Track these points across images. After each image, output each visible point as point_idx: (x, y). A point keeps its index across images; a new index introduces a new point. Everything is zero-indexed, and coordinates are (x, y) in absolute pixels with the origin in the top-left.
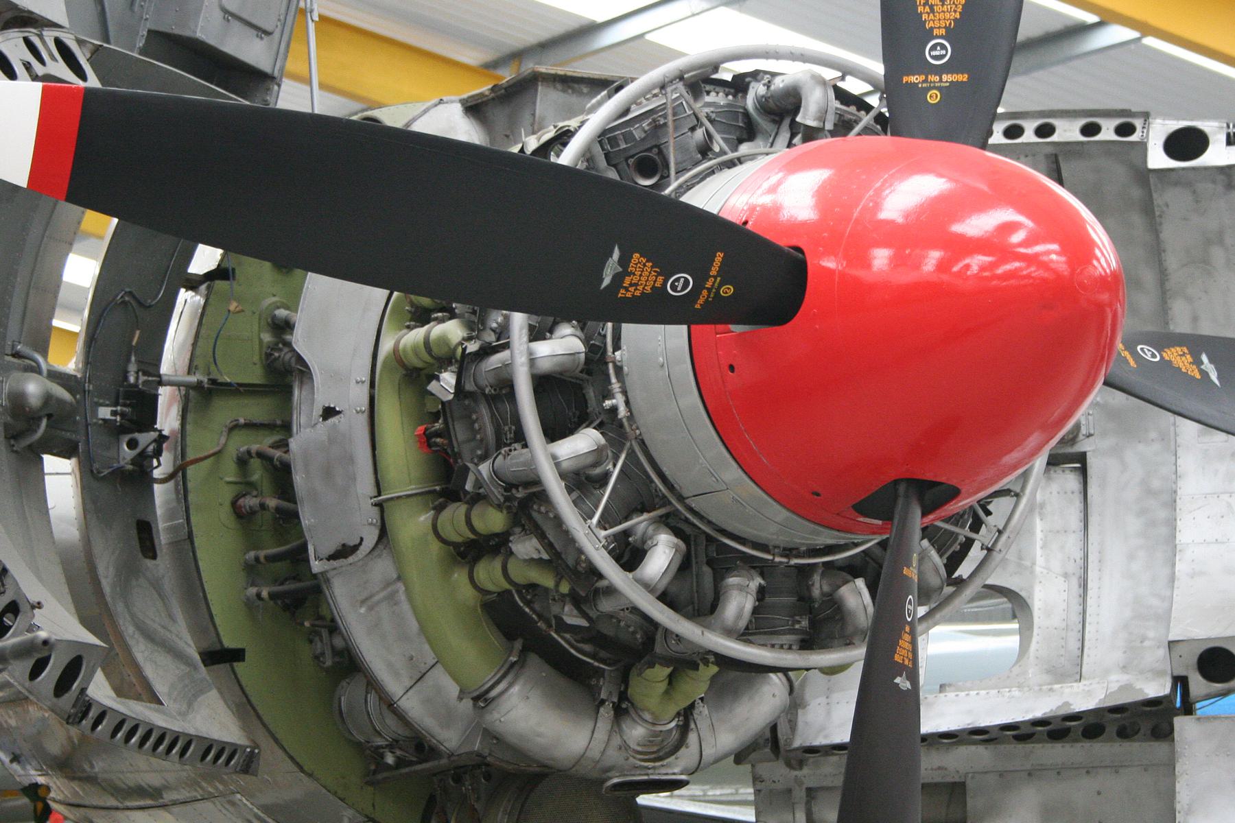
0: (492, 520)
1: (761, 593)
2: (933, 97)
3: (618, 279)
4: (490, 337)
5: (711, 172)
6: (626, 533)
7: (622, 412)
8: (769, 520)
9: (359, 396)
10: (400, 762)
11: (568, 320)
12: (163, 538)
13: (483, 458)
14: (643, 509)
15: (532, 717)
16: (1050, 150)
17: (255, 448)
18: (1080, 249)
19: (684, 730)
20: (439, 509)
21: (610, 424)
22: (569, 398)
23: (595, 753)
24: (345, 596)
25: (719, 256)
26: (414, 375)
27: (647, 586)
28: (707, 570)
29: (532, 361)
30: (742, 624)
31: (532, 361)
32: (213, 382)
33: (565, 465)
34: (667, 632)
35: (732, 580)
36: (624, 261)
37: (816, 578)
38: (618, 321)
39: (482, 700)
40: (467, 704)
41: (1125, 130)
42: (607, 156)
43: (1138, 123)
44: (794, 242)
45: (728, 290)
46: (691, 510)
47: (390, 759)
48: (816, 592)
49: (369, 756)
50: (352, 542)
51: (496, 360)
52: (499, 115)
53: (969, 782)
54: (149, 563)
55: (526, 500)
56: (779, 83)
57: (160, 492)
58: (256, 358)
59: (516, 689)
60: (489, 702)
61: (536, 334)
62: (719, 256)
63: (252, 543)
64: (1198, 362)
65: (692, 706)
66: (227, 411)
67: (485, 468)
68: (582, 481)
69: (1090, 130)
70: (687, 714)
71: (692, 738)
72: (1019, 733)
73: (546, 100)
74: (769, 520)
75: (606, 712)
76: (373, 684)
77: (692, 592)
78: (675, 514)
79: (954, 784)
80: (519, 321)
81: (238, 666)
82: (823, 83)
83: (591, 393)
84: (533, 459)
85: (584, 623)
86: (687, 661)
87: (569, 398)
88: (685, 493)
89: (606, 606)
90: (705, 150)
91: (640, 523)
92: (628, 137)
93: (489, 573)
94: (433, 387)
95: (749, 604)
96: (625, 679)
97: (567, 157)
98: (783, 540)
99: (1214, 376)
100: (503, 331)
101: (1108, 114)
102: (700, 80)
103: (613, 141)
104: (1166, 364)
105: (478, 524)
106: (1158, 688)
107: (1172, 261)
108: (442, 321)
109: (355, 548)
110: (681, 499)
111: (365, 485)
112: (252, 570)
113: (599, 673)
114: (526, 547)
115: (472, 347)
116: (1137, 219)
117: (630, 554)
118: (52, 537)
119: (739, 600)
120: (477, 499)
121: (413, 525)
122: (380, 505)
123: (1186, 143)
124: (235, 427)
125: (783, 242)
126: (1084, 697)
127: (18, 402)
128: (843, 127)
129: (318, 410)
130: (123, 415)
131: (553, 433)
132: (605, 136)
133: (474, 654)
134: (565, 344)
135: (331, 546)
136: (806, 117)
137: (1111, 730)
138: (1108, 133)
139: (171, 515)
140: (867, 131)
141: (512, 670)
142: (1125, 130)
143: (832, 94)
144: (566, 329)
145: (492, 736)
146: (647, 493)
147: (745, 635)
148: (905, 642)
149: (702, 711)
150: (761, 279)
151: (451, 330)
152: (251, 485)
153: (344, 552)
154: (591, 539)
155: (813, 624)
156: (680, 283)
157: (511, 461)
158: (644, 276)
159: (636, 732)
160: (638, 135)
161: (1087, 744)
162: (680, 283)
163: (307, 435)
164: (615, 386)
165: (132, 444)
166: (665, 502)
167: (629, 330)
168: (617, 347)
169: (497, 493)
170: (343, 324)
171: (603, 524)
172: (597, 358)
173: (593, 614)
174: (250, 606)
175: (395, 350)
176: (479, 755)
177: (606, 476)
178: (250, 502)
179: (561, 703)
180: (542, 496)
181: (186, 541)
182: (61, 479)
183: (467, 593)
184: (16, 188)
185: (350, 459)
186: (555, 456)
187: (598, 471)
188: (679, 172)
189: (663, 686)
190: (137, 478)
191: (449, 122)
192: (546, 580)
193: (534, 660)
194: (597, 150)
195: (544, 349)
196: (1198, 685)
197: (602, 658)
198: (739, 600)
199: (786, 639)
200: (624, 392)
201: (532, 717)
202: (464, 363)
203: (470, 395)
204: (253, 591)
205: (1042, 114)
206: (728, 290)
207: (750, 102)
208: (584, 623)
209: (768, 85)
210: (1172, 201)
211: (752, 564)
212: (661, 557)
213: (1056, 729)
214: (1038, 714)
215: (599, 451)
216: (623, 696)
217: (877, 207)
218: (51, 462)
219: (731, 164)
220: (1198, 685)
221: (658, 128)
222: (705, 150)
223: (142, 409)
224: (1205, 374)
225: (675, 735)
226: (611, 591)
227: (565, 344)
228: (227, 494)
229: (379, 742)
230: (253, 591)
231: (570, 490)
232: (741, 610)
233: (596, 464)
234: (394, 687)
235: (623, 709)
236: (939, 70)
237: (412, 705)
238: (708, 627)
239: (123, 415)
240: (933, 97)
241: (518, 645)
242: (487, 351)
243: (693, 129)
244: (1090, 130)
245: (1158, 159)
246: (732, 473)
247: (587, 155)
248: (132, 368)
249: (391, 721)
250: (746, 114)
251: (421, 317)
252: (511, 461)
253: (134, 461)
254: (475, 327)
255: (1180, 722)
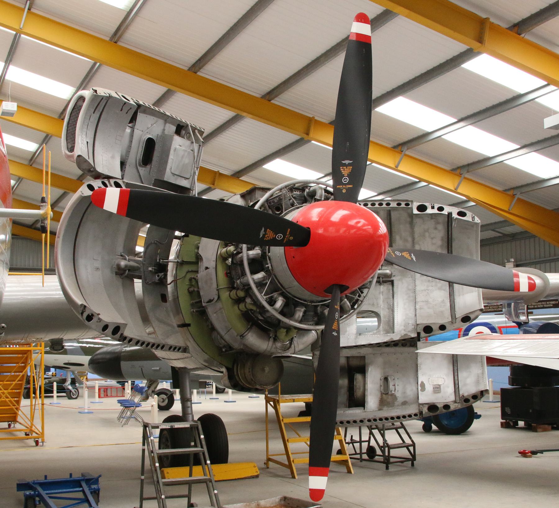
0: (241, 294)
1: (305, 312)
2: (344, 191)
3: (264, 235)
4: (239, 250)
5: (294, 210)
6: (272, 297)
7: (270, 267)
8: (305, 294)
9: (213, 264)
10: (226, 351)
11: (258, 246)
12: (170, 297)
13: (238, 279)
14: (276, 291)
15: (254, 341)
16: (389, 209)
17: (192, 276)
18: (376, 227)
19: (291, 344)
20: (231, 291)
21: (267, 271)
22: (257, 265)
23: (269, 349)
24: (210, 311)
25: (289, 230)
26: (224, 259)
27: (276, 310)
28: (293, 306)
29: (248, 255)
30: (300, 319)
31: (248, 255)
32: (183, 261)
33: (256, 281)
34: (283, 322)
35: (298, 309)
36: (265, 231)
37: (319, 308)
38: (270, 246)
39: (242, 336)
40: (239, 337)
41: (407, 205)
42: (269, 206)
43: (410, 203)
44: (308, 226)
45: (291, 238)
46: (287, 291)
47: (224, 350)
48: (319, 311)
49: (220, 349)
50: (212, 299)
51: (240, 255)
52: (248, 197)
53: (366, 357)
54: (164, 303)
55: (247, 288)
56: (312, 189)
57: (170, 288)
58: (194, 256)
59: (250, 334)
60: (243, 337)
61: (249, 249)
62: (289, 230)
63: (192, 299)
64: (411, 256)
65: (293, 338)
66: (186, 268)
67: (238, 281)
68: (260, 285)
69: (399, 204)
70: (291, 340)
71: (293, 346)
72: (379, 345)
73: (258, 193)
74: (305, 294)
75: (272, 340)
76: (219, 333)
77: (287, 311)
78: (283, 292)
79: (361, 357)
80: (244, 246)
81: (189, 328)
82: (321, 188)
83: (264, 263)
84: (248, 280)
85: (262, 318)
86: (289, 329)
87: (257, 265)
88: (286, 287)
89: (268, 315)
90: (293, 205)
91: (275, 295)
92: (273, 202)
93: (242, 306)
94: (227, 262)
95: (301, 314)
96: (276, 332)
97: (257, 207)
98: (309, 299)
99: (414, 259)
100: (241, 249)
101: (403, 201)
102: (292, 188)
103: (270, 203)
104: (402, 256)
105: (238, 295)
106: (414, 335)
107: (416, 236)
108: (230, 246)
109: (213, 300)
110: (285, 289)
111: (215, 286)
112: (193, 305)
113: (270, 330)
114: (248, 300)
115: (235, 252)
116: (408, 225)
117: (272, 302)
118: (135, 296)
119: (299, 314)
120: (238, 289)
121: (225, 295)
122: (217, 290)
123: (422, 208)
124: (188, 272)
125: (305, 226)
126: (396, 337)
127: (118, 266)
128: (327, 199)
129: (204, 268)
130: (155, 269)
131: (253, 272)
132: (267, 201)
133: (240, 326)
134: (257, 251)
135: (207, 300)
136: (317, 197)
137: (400, 344)
138: (403, 205)
139: (173, 293)
140: (332, 200)
141: (249, 329)
142: (407, 205)
143: (323, 191)
144: (257, 248)
145: (244, 345)
146: (276, 288)
147: (301, 322)
148: (335, 324)
149: (295, 339)
150: (300, 235)
151: (231, 248)
152: (192, 285)
153: (210, 301)
154: (262, 298)
155: (318, 319)
156: (279, 237)
157: (243, 280)
158: (270, 234)
159: (279, 345)
160: (276, 201)
161: (395, 348)
162: (279, 237)
163: (202, 274)
164: (269, 262)
165: (158, 276)
166: (281, 290)
167: (272, 248)
168: (269, 252)
169: (241, 287)
170: (210, 248)
171: (265, 295)
172: (264, 255)
173: (265, 316)
174: (192, 313)
175: (220, 253)
176: (242, 349)
177: (267, 283)
178: (191, 289)
179: (260, 337)
180: (250, 288)
181: (176, 299)
182: (138, 284)
183: (238, 312)
184: (112, 213)
185: (211, 279)
186: (253, 279)
187: (264, 282)
188: (285, 210)
189: (285, 334)
190: (163, 282)
191: (237, 200)
192: (254, 308)
193: (254, 327)
194: (266, 204)
195: (251, 252)
196: (423, 334)
197: (268, 327)
198: (299, 314)
199: (311, 323)
200: (271, 263)
201: (254, 341)
202: (232, 255)
203: (235, 264)
204: (192, 310)
205: (407, 201)
206: (291, 238)
207: (305, 193)
208: (262, 318)
209: (309, 189)
210: (417, 221)
211: (303, 305)
212: (279, 303)
213: (387, 344)
214: (385, 341)
215: (264, 277)
216: (276, 336)
217: (330, 218)
218: (136, 280)
219: (298, 208)
220: (423, 334)
221: (280, 200)
222: (293, 205)
223: (163, 268)
224: (412, 259)
225: (289, 345)
226: (268, 311)
227: (257, 251)
228: (187, 287)
229: (221, 346)
230: (192, 310)
231: (257, 287)
232: (299, 316)
233: (264, 280)
234: (223, 333)
235: (275, 339)
236: (345, 184)
237: (227, 337)
238: (291, 320)
239: (155, 269)
240: (344, 191)
241: (250, 324)
242: (239, 253)
243: (290, 200)
244: (399, 204)
245: (415, 212)
246: (296, 283)
247: (262, 206)
248: (158, 258)
249: (223, 342)
250: (305, 196)
251: (226, 245)
252: (243, 280)
253: (159, 280)
254: (236, 247)
255: (418, 343)
